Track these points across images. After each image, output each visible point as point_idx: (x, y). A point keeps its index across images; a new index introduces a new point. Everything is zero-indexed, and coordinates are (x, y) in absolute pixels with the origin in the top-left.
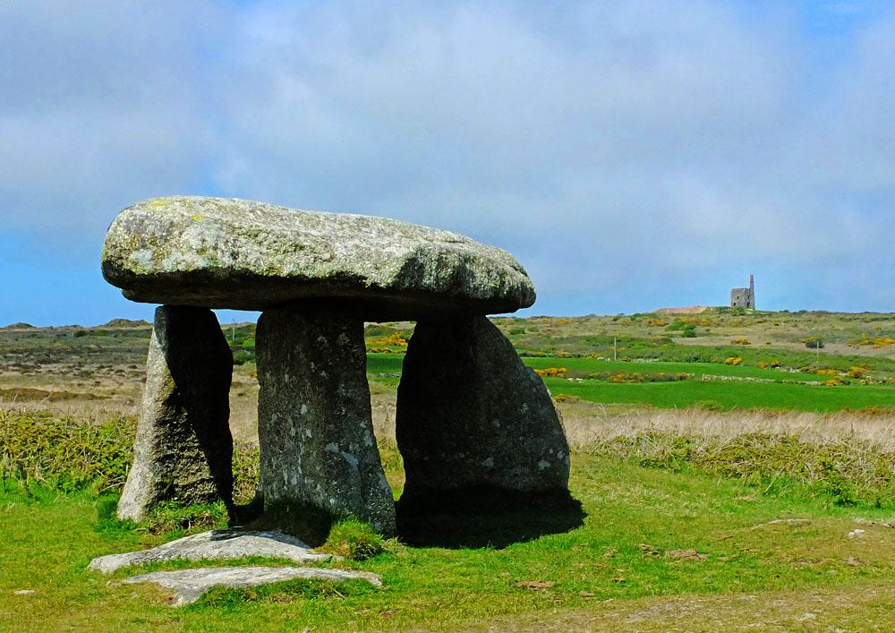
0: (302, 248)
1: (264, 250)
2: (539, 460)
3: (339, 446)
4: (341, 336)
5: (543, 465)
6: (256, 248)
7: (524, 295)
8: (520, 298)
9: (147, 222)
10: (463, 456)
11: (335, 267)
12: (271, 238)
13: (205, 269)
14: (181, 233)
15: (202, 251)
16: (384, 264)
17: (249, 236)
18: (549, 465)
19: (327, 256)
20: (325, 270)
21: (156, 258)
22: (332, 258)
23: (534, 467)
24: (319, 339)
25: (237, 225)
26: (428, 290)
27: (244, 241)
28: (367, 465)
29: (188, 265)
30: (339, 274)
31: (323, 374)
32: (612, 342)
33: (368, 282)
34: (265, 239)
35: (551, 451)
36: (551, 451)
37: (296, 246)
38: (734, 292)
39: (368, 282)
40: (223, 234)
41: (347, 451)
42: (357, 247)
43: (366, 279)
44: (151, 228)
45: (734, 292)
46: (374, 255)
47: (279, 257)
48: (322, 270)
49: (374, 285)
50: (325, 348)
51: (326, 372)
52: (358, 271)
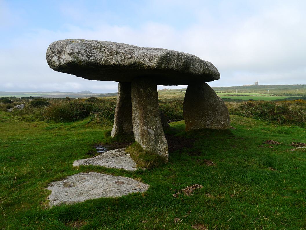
0: (119, 53)
1: (104, 55)
2: (221, 122)
3: (147, 127)
4: (148, 89)
5: (222, 123)
6: (101, 54)
7: (216, 76)
8: (214, 76)
9: (56, 45)
10: (201, 121)
11: (133, 60)
12: (106, 50)
13: (72, 62)
14: (65, 48)
15: (71, 54)
16: (153, 58)
17: (98, 49)
18: (224, 123)
19: (130, 56)
20: (128, 62)
21: (59, 59)
22: (132, 57)
23: (220, 124)
24: (140, 90)
25: (93, 45)
26: (173, 70)
27: (96, 51)
28: (158, 133)
29: (67, 61)
30: (135, 63)
31: (142, 102)
32: (66, 170)
33: (146, 66)
34: (104, 50)
35: (225, 119)
36: (225, 119)
37: (117, 53)
38: (255, 82)
39: (146, 66)
40: (84, 48)
41: (150, 129)
42: (143, 53)
43: (145, 65)
44: (57, 47)
45: (255, 82)
46: (149, 55)
47: (110, 57)
48: (127, 62)
49: (148, 67)
50: (143, 93)
51: (143, 101)
52: (142, 61)
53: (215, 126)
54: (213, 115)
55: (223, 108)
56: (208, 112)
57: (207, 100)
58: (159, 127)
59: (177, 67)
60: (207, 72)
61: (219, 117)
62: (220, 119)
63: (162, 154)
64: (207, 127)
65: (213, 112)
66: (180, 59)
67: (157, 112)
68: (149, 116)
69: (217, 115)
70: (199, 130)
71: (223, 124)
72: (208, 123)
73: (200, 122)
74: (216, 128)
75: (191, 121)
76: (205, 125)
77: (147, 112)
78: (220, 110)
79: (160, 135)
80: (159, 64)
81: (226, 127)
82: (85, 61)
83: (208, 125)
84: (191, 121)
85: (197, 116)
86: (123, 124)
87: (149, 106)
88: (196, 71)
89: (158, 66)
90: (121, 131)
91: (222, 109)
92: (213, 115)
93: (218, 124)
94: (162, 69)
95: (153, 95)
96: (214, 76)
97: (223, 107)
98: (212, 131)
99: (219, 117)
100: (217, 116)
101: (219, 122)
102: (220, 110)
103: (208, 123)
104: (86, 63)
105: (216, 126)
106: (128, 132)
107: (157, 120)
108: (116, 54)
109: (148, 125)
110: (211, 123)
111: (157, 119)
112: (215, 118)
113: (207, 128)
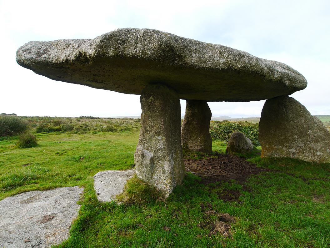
2: (317, 151)
4: (150, 97)
8: (301, 85)
10: (281, 147)
23: (314, 154)
28: (158, 157)
41: (147, 149)
53: (305, 156)
54: (302, 141)
55: (321, 132)
56: (292, 136)
57: (292, 120)
58: (161, 149)
59: (144, 52)
60: (238, 66)
61: (312, 145)
62: (315, 148)
63: (161, 186)
64: (291, 156)
65: (302, 137)
66: (150, 39)
67: (160, 128)
68: (149, 132)
69: (309, 142)
70: (278, 159)
71: (320, 156)
72: (293, 150)
73: (281, 149)
74: (307, 160)
75: (267, 146)
76: (288, 153)
77: (146, 127)
78: (315, 135)
79: (161, 160)
80: (99, 48)
81: (325, 159)
82: (29, 59)
83: (294, 154)
84: (267, 146)
85: (276, 141)
86: (187, 141)
87: (150, 119)
88: (205, 62)
89: (100, 52)
90: (184, 148)
91: (319, 133)
92: (302, 141)
93: (310, 154)
94: (111, 56)
95: (155, 105)
96: (301, 85)
97: (320, 131)
98: (299, 162)
99: (312, 145)
100: (308, 143)
101: (312, 152)
102: (315, 135)
103: (293, 150)
104: (32, 62)
105: (307, 157)
106: (192, 150)
107: (160, 139)
108: (67, 47)
109: (146, 144)
110: (298, 151)
111: (159, 138)
112: (305, 145)
113: (292, 157)
